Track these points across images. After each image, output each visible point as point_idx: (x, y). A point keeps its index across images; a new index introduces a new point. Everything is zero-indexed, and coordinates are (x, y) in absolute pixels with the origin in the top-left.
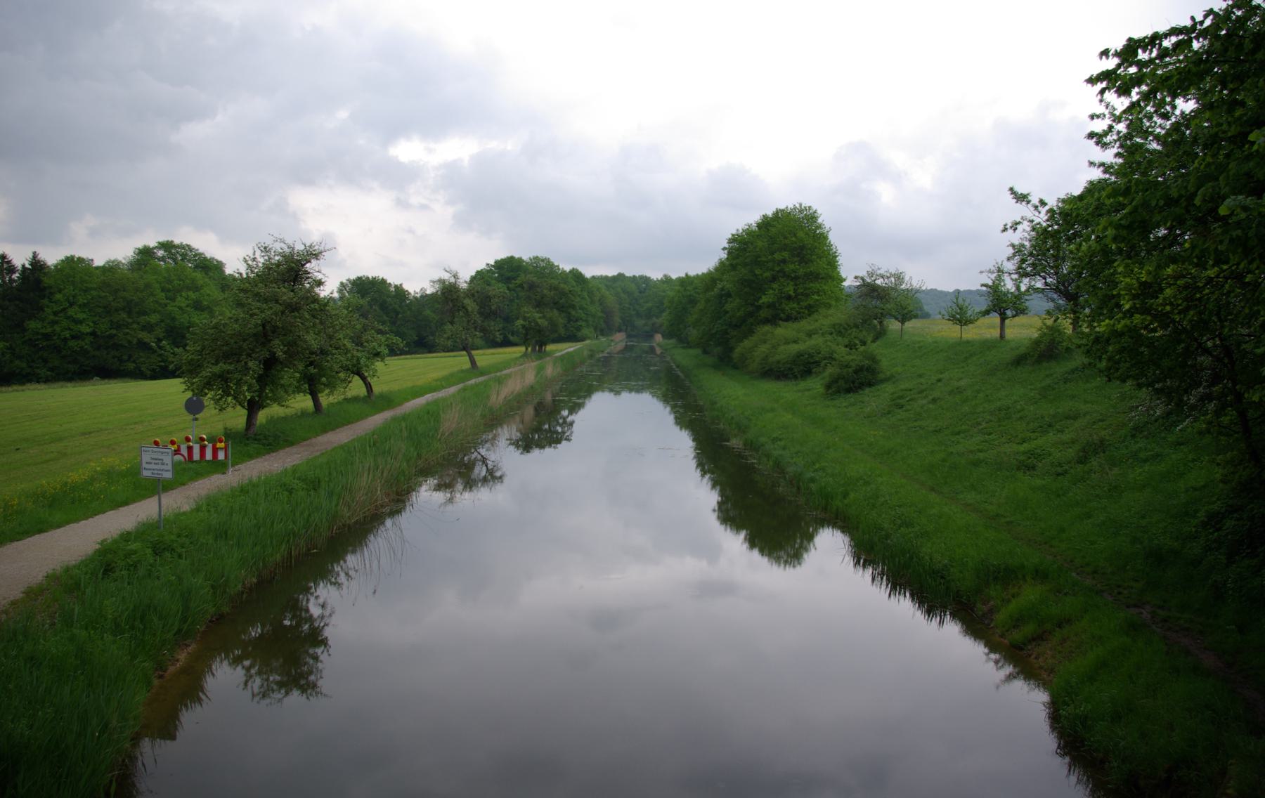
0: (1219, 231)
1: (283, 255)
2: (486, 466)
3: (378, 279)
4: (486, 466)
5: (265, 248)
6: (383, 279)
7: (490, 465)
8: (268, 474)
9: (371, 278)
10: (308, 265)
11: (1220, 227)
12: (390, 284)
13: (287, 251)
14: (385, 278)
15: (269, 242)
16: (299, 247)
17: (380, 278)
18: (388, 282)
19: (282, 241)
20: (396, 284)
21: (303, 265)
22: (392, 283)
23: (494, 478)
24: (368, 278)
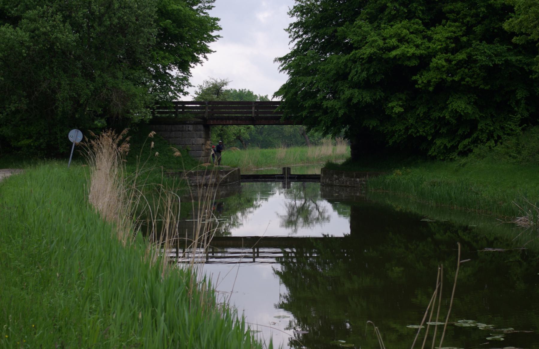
0: (447, 115)
1: (213, 84)
2: (319, 211)
3: (245, 92)
4: (319, 211)
5: (207, 82)
6: (249, 91)
7: (321, 210)
8: (244, 193)
9: (238, 91)
10: (222, 88)
11: (175, 177)
12: (256, 96)
13: (214, 82)
14: (251, 90)
15: (208, 80)
16: (219, 81)
17: (247, 90)
18: (254, 94)
19: (213, 79)
20: (261, 95)
21: (221, 88)
22: (258, 95)
23: (323, 219)
24: (236, 91)
